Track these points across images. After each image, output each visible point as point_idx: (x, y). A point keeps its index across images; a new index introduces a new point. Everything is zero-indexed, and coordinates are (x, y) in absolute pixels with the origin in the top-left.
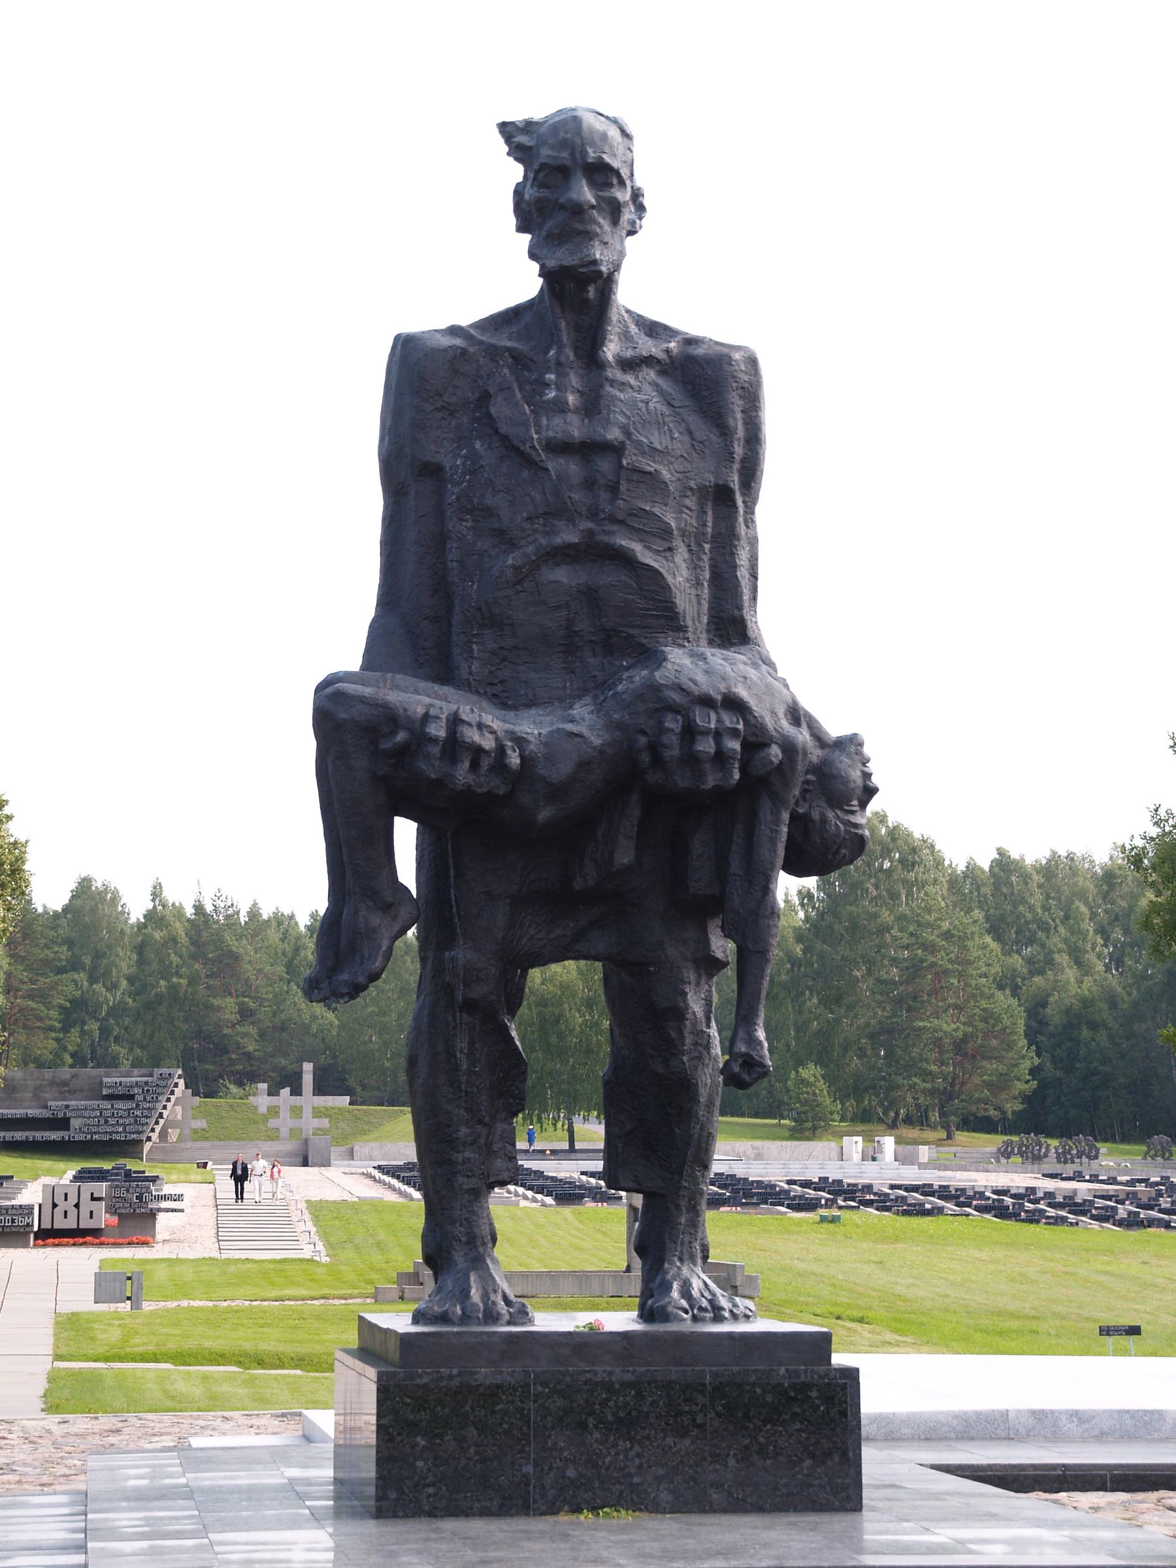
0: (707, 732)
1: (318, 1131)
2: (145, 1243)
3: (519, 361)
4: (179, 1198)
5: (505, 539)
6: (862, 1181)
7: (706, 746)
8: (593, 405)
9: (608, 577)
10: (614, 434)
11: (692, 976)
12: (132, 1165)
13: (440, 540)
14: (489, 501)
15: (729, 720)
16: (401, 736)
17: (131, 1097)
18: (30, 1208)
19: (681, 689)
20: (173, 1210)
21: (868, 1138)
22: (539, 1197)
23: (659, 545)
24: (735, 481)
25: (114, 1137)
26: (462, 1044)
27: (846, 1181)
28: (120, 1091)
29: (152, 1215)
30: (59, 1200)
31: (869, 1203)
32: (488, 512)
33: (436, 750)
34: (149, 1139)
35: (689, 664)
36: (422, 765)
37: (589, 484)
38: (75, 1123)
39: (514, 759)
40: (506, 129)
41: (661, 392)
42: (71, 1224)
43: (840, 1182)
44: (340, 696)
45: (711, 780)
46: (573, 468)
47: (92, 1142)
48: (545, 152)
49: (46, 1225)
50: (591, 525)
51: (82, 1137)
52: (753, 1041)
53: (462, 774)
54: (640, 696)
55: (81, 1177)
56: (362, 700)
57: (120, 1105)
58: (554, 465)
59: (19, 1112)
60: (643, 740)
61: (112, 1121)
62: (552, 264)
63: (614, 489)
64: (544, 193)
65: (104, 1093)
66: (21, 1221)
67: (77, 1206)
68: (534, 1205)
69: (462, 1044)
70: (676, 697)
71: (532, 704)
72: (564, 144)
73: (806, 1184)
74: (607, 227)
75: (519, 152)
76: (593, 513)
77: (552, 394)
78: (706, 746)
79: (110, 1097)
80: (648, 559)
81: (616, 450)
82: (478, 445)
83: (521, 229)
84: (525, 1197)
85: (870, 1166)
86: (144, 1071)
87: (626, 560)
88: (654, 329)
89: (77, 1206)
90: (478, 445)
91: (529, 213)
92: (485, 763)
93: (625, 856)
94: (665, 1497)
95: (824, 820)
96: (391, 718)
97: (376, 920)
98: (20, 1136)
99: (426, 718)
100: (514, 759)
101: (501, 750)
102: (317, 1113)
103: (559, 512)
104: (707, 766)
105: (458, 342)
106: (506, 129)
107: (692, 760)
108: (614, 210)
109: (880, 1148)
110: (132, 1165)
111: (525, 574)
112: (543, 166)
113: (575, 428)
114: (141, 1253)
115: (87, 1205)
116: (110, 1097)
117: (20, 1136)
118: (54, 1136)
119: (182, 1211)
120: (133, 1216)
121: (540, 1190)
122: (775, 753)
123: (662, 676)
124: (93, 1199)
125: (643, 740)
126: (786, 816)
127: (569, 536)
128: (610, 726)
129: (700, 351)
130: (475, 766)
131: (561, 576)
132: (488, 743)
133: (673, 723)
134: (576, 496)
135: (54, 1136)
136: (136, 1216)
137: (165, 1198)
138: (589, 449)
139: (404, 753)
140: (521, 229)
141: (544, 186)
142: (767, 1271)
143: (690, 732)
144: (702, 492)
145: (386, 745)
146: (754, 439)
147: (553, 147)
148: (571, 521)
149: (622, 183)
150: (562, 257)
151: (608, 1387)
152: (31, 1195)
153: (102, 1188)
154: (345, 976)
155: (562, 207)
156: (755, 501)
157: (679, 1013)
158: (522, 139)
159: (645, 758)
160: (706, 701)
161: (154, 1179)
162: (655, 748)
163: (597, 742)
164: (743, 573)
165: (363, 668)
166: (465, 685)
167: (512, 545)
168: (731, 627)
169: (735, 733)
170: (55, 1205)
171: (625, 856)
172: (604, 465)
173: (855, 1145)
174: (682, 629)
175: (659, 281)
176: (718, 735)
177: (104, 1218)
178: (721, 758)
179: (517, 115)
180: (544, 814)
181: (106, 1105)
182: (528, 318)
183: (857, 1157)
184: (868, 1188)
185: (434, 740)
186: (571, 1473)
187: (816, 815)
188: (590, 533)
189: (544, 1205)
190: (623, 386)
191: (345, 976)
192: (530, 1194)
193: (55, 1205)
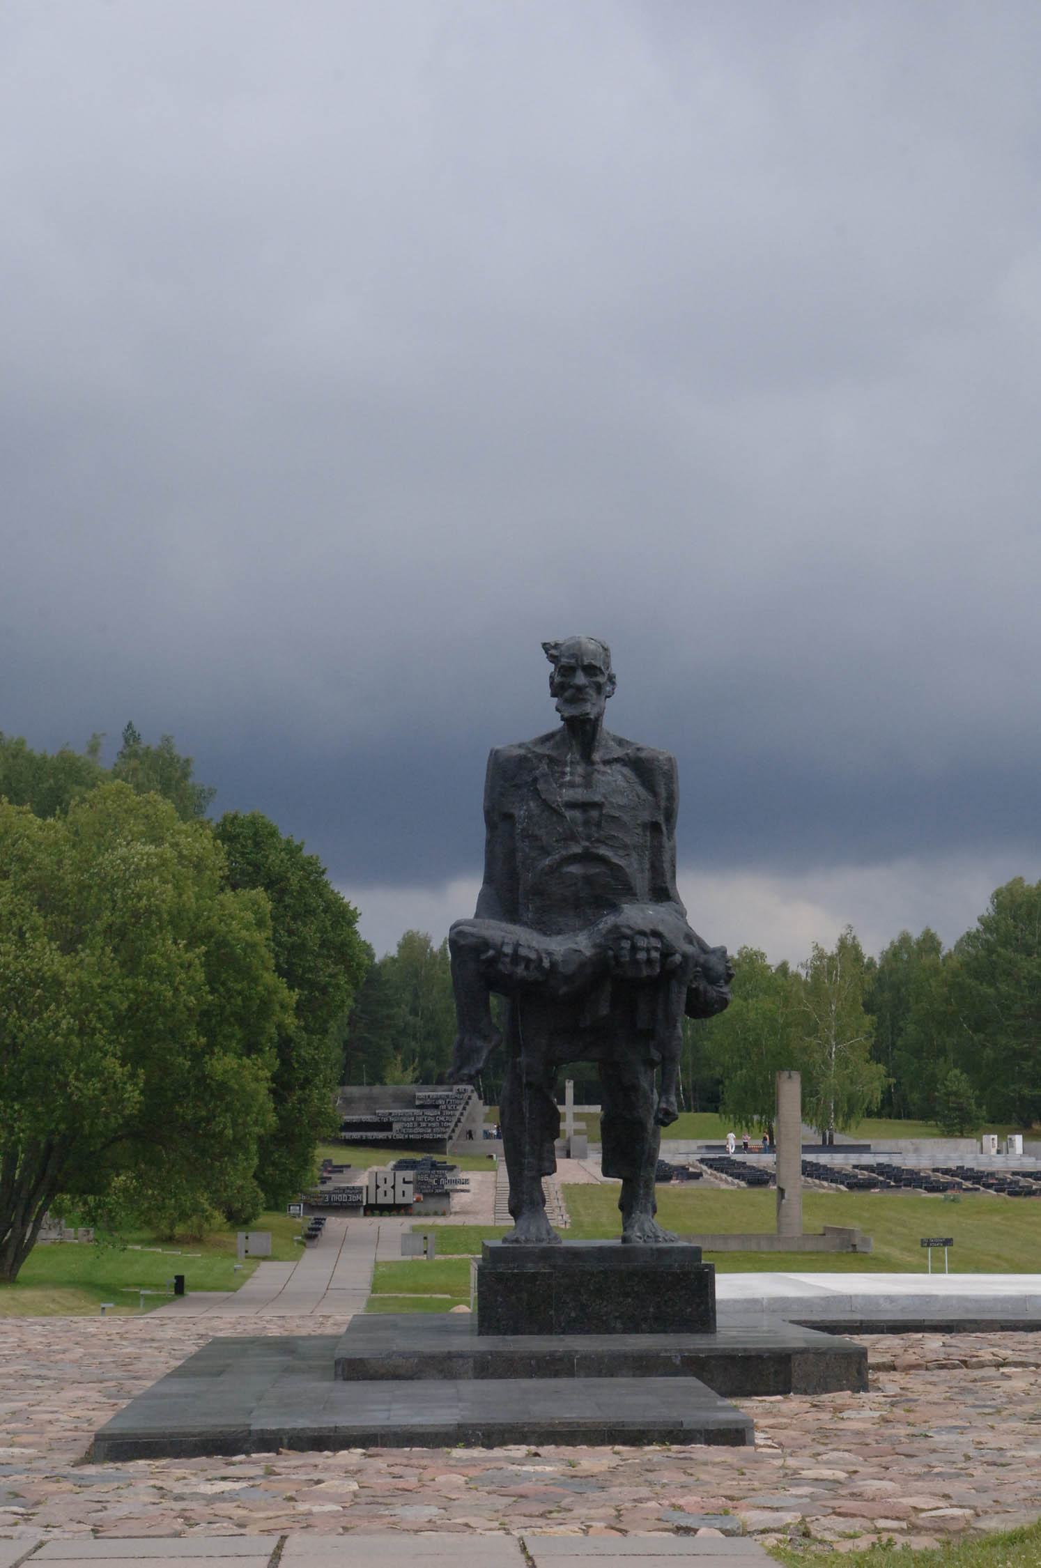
0: (642, 949)
1: (577, 1132)
2: (444, 1214)
3: (552, 761)
4: (466, 1182)
5: (545, 851)
6: (990, 1169)
7: (642, 956)
8: (588, 783)
9: (594, 870)
10: (598, 798)
11: (642, 1069)
12: (437, 1158)
13: (512, 852)
14: (537, 832)
15: (655, 942)
16: (491, 953)
17: (437, 1107)
18: (360, 1189)
19: (629, 927)
20: (463, 1191)
21: (1002, 1137)
22: (736, 1181)
23: (621, 852)
24: (661, 819)
25: (426, 1136)
26: (526, 1104)
27: (976, 1169)
28: (429, 1102)
29: (447, 1195)
30: (381, 1183)
31: (988, 1186)
32: (536, 838)
33: (508, 960)
34: (450, 1138)
35: (638, 914)
36: (501, 967)
37: (586, 823)
38: (396, 1127)
39: (546, 964)
40: (546, 646)
41: (624, 776)
42: (389, 1200)
43: (972, 1170)
44: (460, 933)
45: (645, 972)
46: (577, 814)
47: (409, 1140)
48: (564, 660)
49: (372, 1201)
50: (587, 844)
51: (401, 1137)
52: (668, 1102)
53: (520, 970)
54: (610, 931)
55: (401, 1166)
56: (472, 935)
57: (429, 1112)
58: (569, 814)
59: (355, 1118)
60: (611, 953)
61: (424, 1125)
62: (566, 715)
63: (598, 825)
64: (563, 679)
65: (417, 1103)
66: (354, 1198)
67: (393, 1187)
68: (732, 1188)
69: (526, 1104)
70: (628, 932)
71: (559, 933)
72: (573, 656)
73: (946, 1172)
74: (595, 695)
75: (553, 659)
76: (588, 838)
77: (568, 778)
78: (642, 956)
79: (421, 1107)
80: (616, 860)
81: (598, 806)
82: (532, 804)
83: (553, 695)
84: (727, 1182)
85: (1000, 1158)
86: (446, 1087)
87: (603, 860)
88: (621, 742)
89: (393, 1187)
90: (532, 804)
91: (558, 689)
92: (532, 966)
93: (604, 1011)
94: (619, 1325)
95: (706, 992)
96: (485, 944)
97: (479, 1043)
98: (356, 1135)
99: (503, 944)
100: (546, 964)
101: (540, 959)
102: (578, 1117)
103: (572, 837)
104: (643, 966)
105: (522, 752)
106: (546, 646)
107: (635, 962)
108: (599, 688)
109: (1011, 1144)
110: (437, 1158)
111: (554, 870)
112: (562, 667)
113: (579, 794)
114: (440, 1221)
115: (400, 1187)
116: (421, 1107)
117: (356, 1135)
118: (381, 1135)
119: (468, 1191)
120: (432, 1195)
121: (737, 1176)
122: (678, 958)
123: (621, 920)
124: (405, 1182)
125: (611, 953)
126: (685, 990)
127: (576, 849)
128: (595, 946)
129: (643, 755)
130: (527, 968)
131: (574, 869)
132: (533, 956)
133: (626, 944)
134: (580, 829)
135: (381, 1135)
136: (435, 1192)
137: (456, 1182)
138: (585, 806)
139: (492, 962)
140: (553, 695)
141: (563, 675)
142: (681, 1215)
143: (634, 949)
144: (645, 826)
145: (483, 957)
146: (671, 797)
147: (568, 657)
148: (577, 842)
149: (602, 673)
150: (571, 711)
151: (592, 1274)
152: (362, 1180)
153: (410, 1175)
154: (466, 1071)
155: (571, 687)
156: (673, 828)
157: (635, 1088)
158: (553, 652)
159: (613, 963)
160: (642, 933)
161: (452, 1168)
162: (616, 957)
163: (588, 954)
164: (666, 866)
165: (477, 916)
166: (524, 924)
167: (549, 854)
168: (662, 893)
169: (656, 949)
170: (378, 1187)
171: (604, 1011)
172: (594, 814)
173: (991, 1141)
174: (635, 895)
175: (620, 717)
176: (648, 950)
177: (410, 1198)
178: (649, 961)
179: (551, 640)
180: (563, 990)
181: (417, 1111)
182: (558, 738)
183: (994, 1151)
184: (991, 1174)
185: (506, 955)
186: (573, 1315)
187: (701, 988)
188: (586, 848)
189: (739, 1187)
190: (604, 773)
191: (466, 1071)
192: (730, 1179)
193: (378, 1187)
